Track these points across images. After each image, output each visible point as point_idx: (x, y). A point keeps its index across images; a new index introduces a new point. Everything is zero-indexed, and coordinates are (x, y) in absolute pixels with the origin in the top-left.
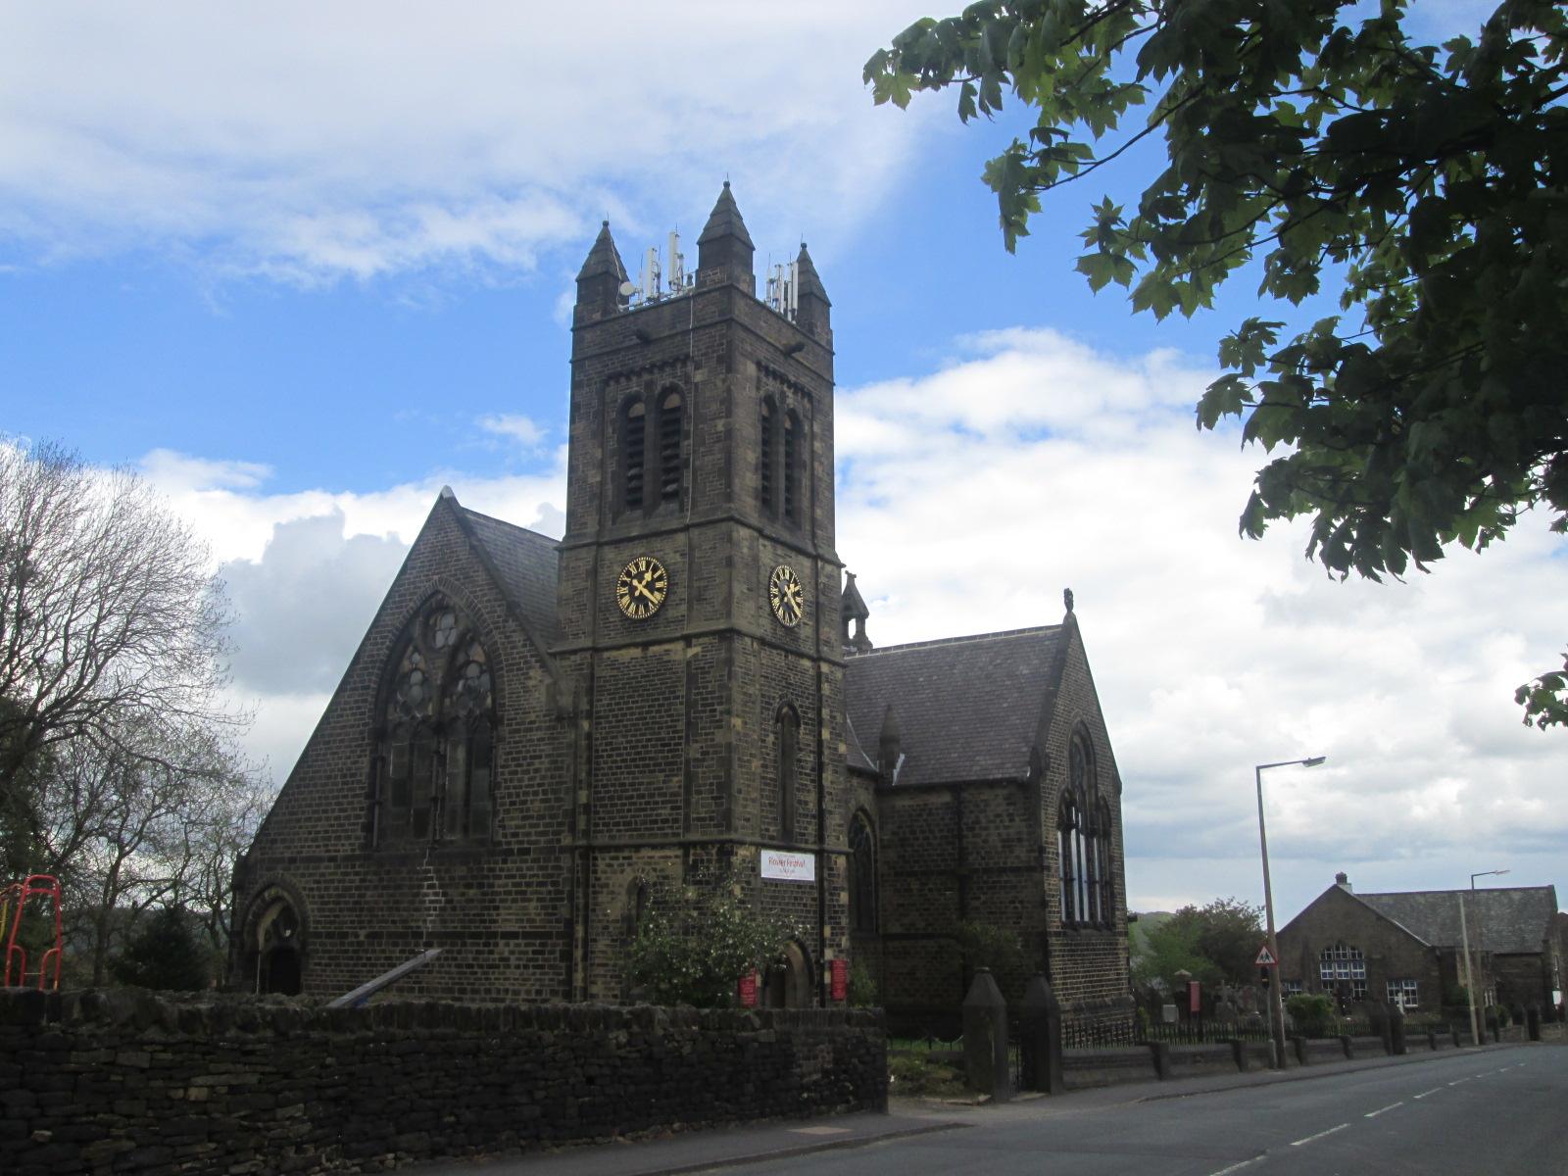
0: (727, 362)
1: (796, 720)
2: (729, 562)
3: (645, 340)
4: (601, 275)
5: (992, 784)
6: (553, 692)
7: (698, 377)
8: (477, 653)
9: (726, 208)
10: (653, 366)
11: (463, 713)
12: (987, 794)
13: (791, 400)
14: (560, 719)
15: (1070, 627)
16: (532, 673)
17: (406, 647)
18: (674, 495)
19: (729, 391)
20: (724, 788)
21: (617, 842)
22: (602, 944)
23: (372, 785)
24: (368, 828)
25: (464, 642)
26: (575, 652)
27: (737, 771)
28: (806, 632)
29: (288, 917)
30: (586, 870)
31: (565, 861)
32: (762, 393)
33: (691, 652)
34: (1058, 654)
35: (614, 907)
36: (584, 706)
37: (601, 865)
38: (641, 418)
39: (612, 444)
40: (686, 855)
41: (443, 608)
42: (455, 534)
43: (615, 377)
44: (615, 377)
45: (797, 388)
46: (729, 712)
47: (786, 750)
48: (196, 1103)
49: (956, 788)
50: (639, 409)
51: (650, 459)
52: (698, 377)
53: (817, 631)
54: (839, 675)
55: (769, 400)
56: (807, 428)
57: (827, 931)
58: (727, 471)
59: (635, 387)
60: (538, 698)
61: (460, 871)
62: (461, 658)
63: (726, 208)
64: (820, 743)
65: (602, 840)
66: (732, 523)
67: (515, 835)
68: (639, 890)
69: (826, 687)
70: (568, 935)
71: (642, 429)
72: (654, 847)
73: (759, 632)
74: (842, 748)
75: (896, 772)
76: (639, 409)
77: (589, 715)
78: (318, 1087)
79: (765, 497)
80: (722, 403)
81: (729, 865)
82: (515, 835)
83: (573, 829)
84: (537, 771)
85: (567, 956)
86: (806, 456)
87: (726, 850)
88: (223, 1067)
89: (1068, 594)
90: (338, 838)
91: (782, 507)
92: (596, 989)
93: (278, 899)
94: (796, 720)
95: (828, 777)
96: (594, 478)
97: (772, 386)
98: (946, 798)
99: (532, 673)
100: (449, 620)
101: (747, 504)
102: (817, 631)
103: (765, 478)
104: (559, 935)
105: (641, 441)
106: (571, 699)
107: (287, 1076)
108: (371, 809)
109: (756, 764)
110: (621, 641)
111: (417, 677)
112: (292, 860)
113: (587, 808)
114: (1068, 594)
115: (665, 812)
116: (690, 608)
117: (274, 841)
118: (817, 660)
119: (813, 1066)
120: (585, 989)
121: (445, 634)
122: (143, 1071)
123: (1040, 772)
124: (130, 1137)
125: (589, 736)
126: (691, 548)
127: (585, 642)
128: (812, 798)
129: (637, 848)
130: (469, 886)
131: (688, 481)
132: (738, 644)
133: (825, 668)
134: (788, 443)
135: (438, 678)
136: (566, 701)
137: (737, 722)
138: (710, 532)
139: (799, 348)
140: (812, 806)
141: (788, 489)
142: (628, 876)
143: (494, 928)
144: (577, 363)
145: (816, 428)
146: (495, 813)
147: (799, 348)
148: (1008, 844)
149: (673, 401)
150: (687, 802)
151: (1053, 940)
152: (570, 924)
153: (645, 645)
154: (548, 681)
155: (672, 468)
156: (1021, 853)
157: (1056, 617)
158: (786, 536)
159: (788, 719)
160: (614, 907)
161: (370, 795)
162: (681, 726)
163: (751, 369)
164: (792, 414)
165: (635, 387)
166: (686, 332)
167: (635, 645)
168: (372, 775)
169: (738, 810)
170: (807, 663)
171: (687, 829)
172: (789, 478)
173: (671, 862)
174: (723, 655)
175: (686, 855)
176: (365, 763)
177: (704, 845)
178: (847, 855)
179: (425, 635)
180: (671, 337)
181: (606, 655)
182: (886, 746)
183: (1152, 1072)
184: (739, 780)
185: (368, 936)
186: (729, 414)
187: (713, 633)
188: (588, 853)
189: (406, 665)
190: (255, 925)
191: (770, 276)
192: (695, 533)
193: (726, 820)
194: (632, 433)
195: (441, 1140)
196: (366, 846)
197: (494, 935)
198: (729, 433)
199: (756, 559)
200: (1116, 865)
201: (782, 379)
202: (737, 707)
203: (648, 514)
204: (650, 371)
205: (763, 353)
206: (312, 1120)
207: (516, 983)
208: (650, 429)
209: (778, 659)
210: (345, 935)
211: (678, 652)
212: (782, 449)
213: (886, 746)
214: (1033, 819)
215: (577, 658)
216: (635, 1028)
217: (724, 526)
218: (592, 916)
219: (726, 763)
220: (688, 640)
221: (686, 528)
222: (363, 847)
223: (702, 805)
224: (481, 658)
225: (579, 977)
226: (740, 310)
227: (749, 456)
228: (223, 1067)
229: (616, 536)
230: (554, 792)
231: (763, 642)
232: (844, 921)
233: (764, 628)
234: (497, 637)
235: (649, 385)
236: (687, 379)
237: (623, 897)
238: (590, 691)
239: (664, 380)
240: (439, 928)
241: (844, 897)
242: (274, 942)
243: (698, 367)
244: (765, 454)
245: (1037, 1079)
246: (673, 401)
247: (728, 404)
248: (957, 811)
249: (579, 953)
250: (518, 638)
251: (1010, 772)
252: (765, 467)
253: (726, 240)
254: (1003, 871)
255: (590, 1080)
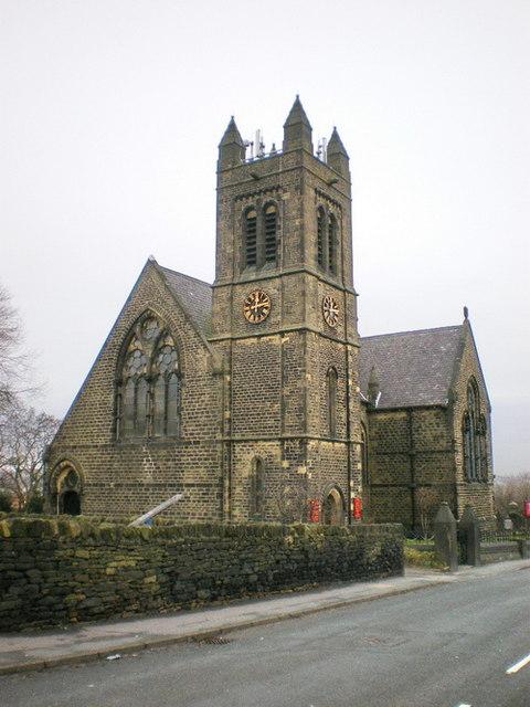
0: (300, 189)
1: (336, 375)
2: (304, 294)
3: (256, 179)
4: (231, 144)
5: (428, 408)
6: (211, 361)
7: (286, 197)
8: (170, 341)
9: (298, 108)
10: (261, 191)
11: (162, 372)
12: (426, 413)
13: (332, 209)
14: (214, 375)
15: (467, 325)
16: (199, 351)
17: (131, 338)
18: (273, 258)
19: (302, 205)
20: (302, 409)
21: (244, 438)
22: (238, 490)
23: (116, 409)
24: (114, 430)
25: (164, 334)
26: (223, 340)
27: (309, 401)
28: (340, 330)
29: (72, 476)
30: (230, 452)
31: (219, 448)
32: (317, 205)
33: (284, 340)
34: (460, 340)
35: (245, 469)
36: (227, 368)
37: (237, 449)
38: (255, 218)
39: (240, 232)
40: (282, 445)
41: (151, 318)
42: (156, 279)
43: (241, 198)
44: (241, 198)
45: (334, 203)
46: (304, 371)
47: (331, 390)
48: (110, 575)
49: (409, 410)
50: (252, 214)
51: (260, 241)
52: (286, 197)
53: (346, 329)
54: (356, 351)
55: (320, 209)
56: (339, 223)
57: (352, 483)
58: (301, 247)
59: (251, 202)
60: (203, 365)
61: (163, 452)
62: (161, 344)
63: (298, 108)
64: (348, 387)
65: (237, 437)
66: (305, 274)
67: (191, 434)
68: (258, 461)
69: (350, 357)
70: (221, 485)
71: (255, 225)
72: (265, 440)
73: (319, 330)
74: (358, 389)
75: (377, 401)
76: (252, 214)
77: (230, 373)
78: (162, 567)
79: (320, 260)
80: (298, 210)
81: (306, 449)
82: (191, 434)
83: (222, 430)
84: (203, 401)
85: (221, 496)
86: (339, 239)
87: (303, 442)
88: (121, 557)
89: (466, 310)
90: (98, 436)
91: (328, 265)
92: (236, 512)
93: (67, 466)
94: (336, 375)
95: (351, 404)
96: (229, 250)
97: (322, 201)
98: (404, 415)
99: (199, 351)
100: (153, 325)
101: (311, 264)
102: (346, 329)
103: (320, 249)
104: (217, 485)
105: (254, 231)
106: (220, 364)
107: (148, 561)
108: (115, 421)
109: (318, 397)
110: (245, 335)
111: (137, 354)
112: (75, 447)
113: (230, 420)
114: (466, 310)
115: (271, 422)
116: (283, 318)
117: (65, 437)
118: (346, 344)
119: (374, 552)
120: (230, 513)
121: (153, 330)
122: (86, 559)
123: (452, 402)
124: (83, 593)
125: (230, 383)
126: (283, 286)
127: (228, 336)
128: (344, 415)
129: (256, 441)
130: (168, 460)
131: (280, 252)
132: (308, 336)
133: (349, 348)
134: (330, 231)
135: (149, 353)
136: (218, 366)
137: (308, 376)
138: (293, 278)
139: (335, 182)
140: (344, 420)
141: (330, 256)
142: (252, 455)
143: (181, 481)
144: (219, 190)
145: (344, 224)
146: (181, 423)
147: (335, 182)
148: (436, 438)
149: (271, 210)
150: (283, 418)
151: (459, 488)
152: (222, 479)
153: (259, 337)
154: (208, 355)
155: (272, 243)
156: (443, 444)
157: (460, 321)
158: (334, 282)
159: (333, 374)
160: (245, 469)
161: (115, 414)
162: (279, 378)
163: (312, 193)
164: (332, 216)
165: (251, 202)
166: (278, 174)
167: (254, 337)
168: (115, 404)
169: (310, 422)
170: (340, 346)
171: (283, 431)
172: (331, 250)
173: (274, 449)
174: (301, 342)
175: (282, 445)
176: (111, 398)
177: (292, 439)
178: (362, 444)
179: (141, 332)
180: (269, 176)
181: (238, 342)
182: (372, 388)
183: (518, 555)
184: (310, 407)
185: (115, 485)
186: (302, 216)
187: (295, 330)
188: (230, 443)
189: (132, 347)
190: (56, 479)
191: (320, 138)
192: (285, 279)
193: (304, 426)
194: (250, 226)
195: (216, 592)
196: (113, 440)
197: (181, 485)
198: (302, 226)
199: (316, 292)
200: (488, 449)
201: (327, 198)
202: (309, 368)
203: (258, 269)
204: (259, 194)
205: (318, 184)
206: (160, 583)
207: (240, 516)
208: (260, 225)
209: (327, 342)
210: (103, 485)
211: (277, 340)
212: (327, 234)
213: (372, 388)
214: (449, 426)
215: (223, 343)
216: (296, 535)
217: (300, 275)
218: (233, 476)
219: (304, 397)
220: (282, 334)
221: (281, 276)
222: (112, 440)
223: (290, 420)
224: (172, 344)
225: (227, 506)
226: (307, 163)
227: (311, 238)
228: (121, 557)
229: (241, 280)
230: (213, 412)
231: (320, 334)
232: (360, 478)
233: (320, 328)
234: (181, 333)
235: (258, 201)
236: (279, 198)
237: (249, 466)
238: (230, 361)
239: (267, 198)
240: (152, 482)
241: (359, 466)
242: (66, 489)
243: (285, 191)
244: (319, 237)
245: (466, 559)
246: (271, 210)
247: (301, 211)
248: (410, 421)
249: (227, 494)
250: (191, 333)
251: (437, 401)
252: (320, 244)
253: (297, 124)
254: (433, 452)
255: (278, 562)
